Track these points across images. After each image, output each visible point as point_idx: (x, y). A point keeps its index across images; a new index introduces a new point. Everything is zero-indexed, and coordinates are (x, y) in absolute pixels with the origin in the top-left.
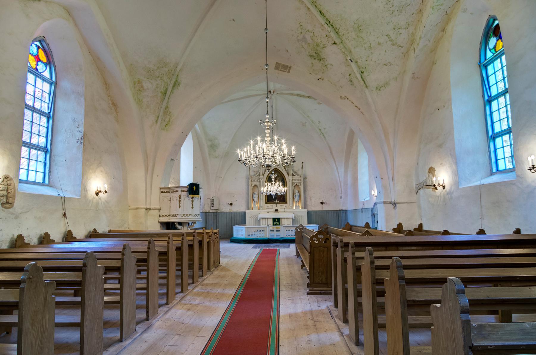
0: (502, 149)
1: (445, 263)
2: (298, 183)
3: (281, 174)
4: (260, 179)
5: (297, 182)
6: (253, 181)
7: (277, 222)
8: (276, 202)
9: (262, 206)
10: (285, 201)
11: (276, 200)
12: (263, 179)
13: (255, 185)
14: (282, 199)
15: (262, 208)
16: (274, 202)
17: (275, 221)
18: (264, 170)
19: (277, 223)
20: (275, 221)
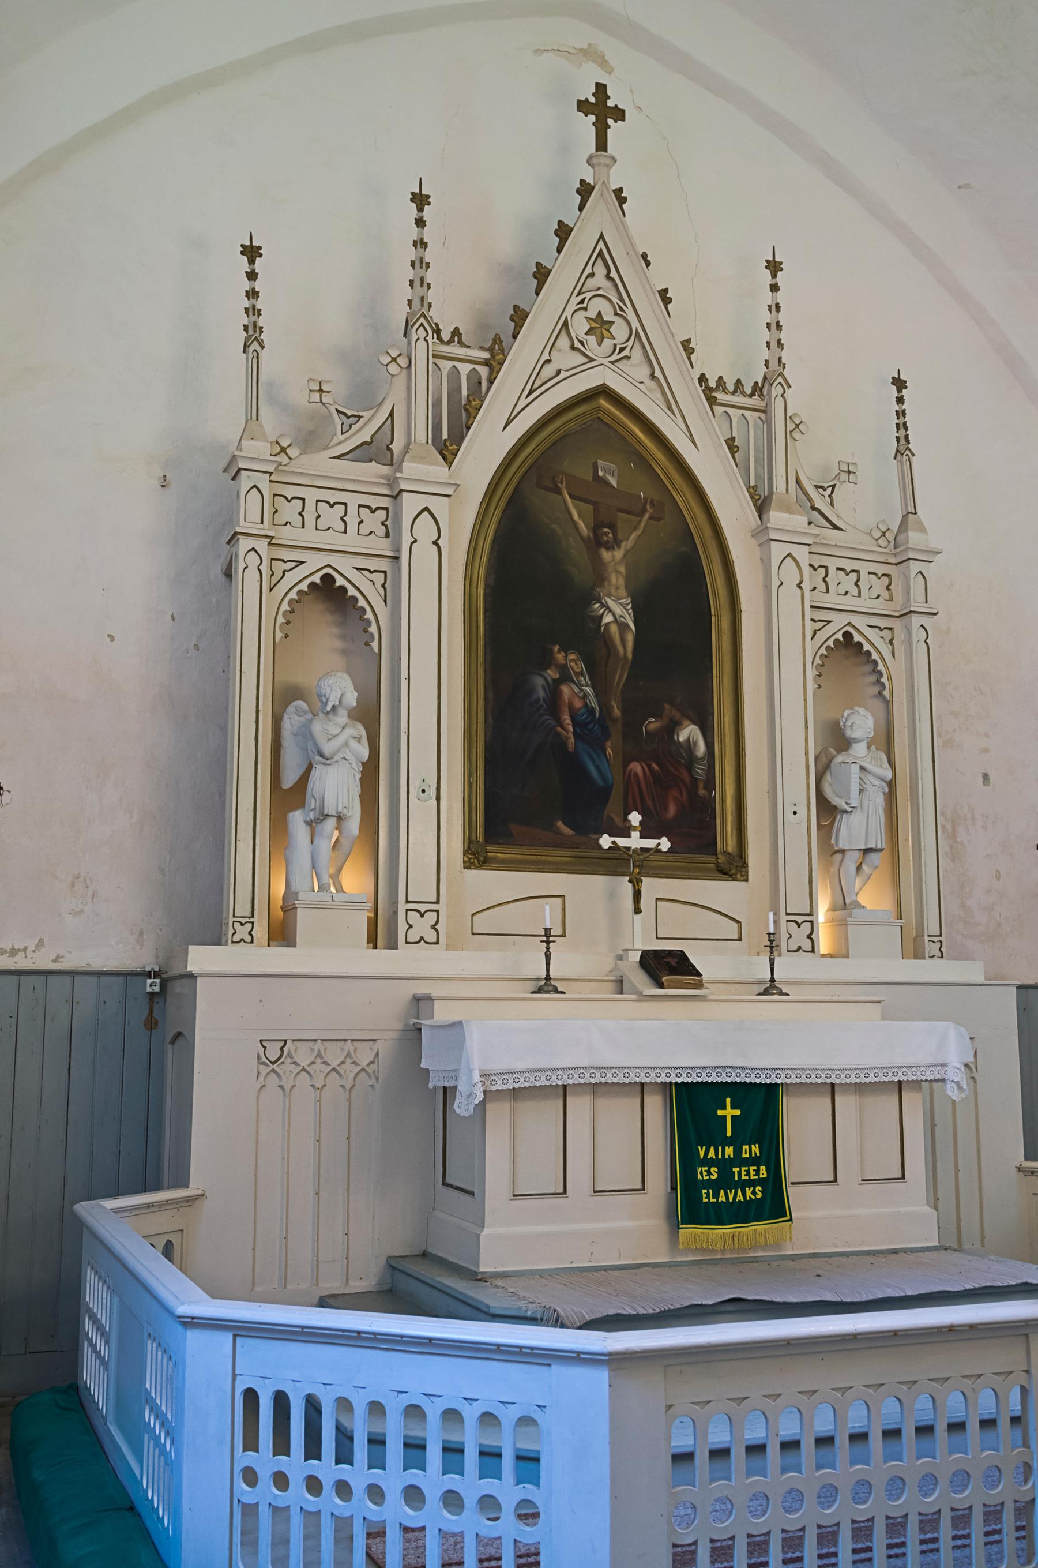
0: (390, 359)
1: (196, 1052)
2: (345, 565)
3: (644, 463)
4: (410, 504)
5: (351, 541)
6: (290, 511)
7: (736, 1142)
8: (635, 841)
9: (422, 888)
10: (708, 845)
11: (635, 818)
12: (438, 506)
13: (847, 635)
14: (672, 810)
15: (422, 927)
16: (606, 841)
17: (713, 1134)
18: (454, 390)
19: (739, 1160)
20: (713, 1134)
